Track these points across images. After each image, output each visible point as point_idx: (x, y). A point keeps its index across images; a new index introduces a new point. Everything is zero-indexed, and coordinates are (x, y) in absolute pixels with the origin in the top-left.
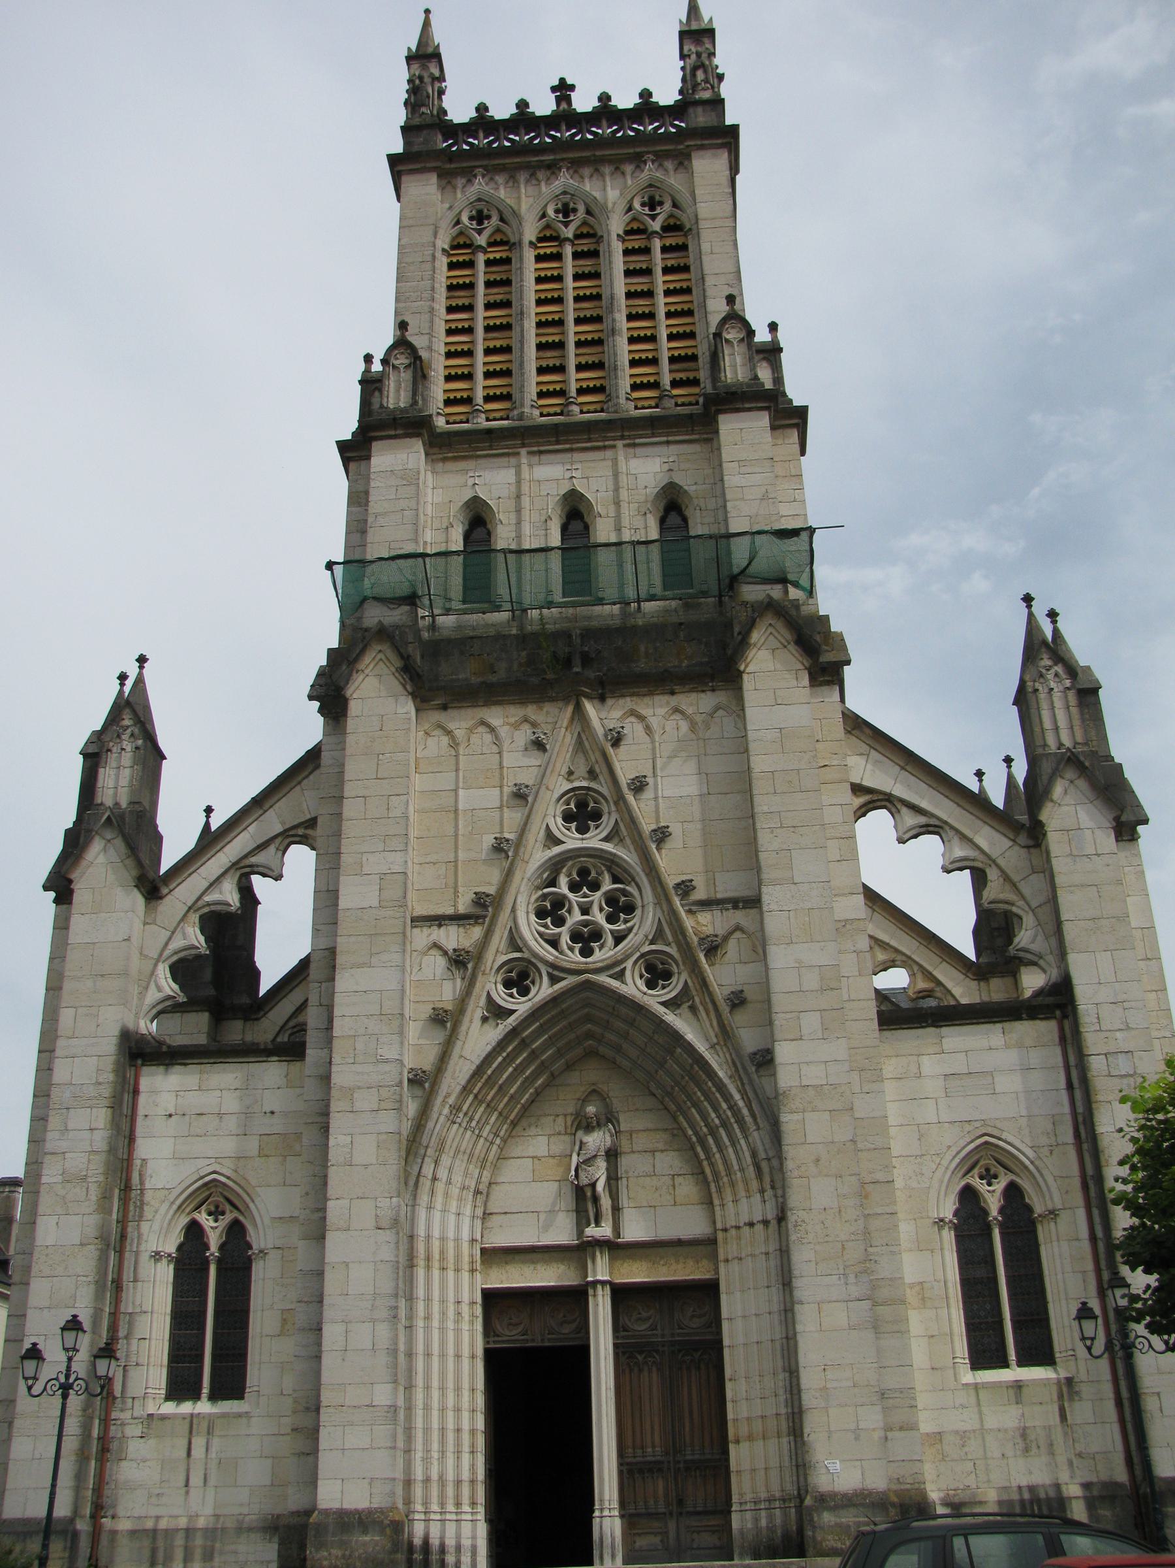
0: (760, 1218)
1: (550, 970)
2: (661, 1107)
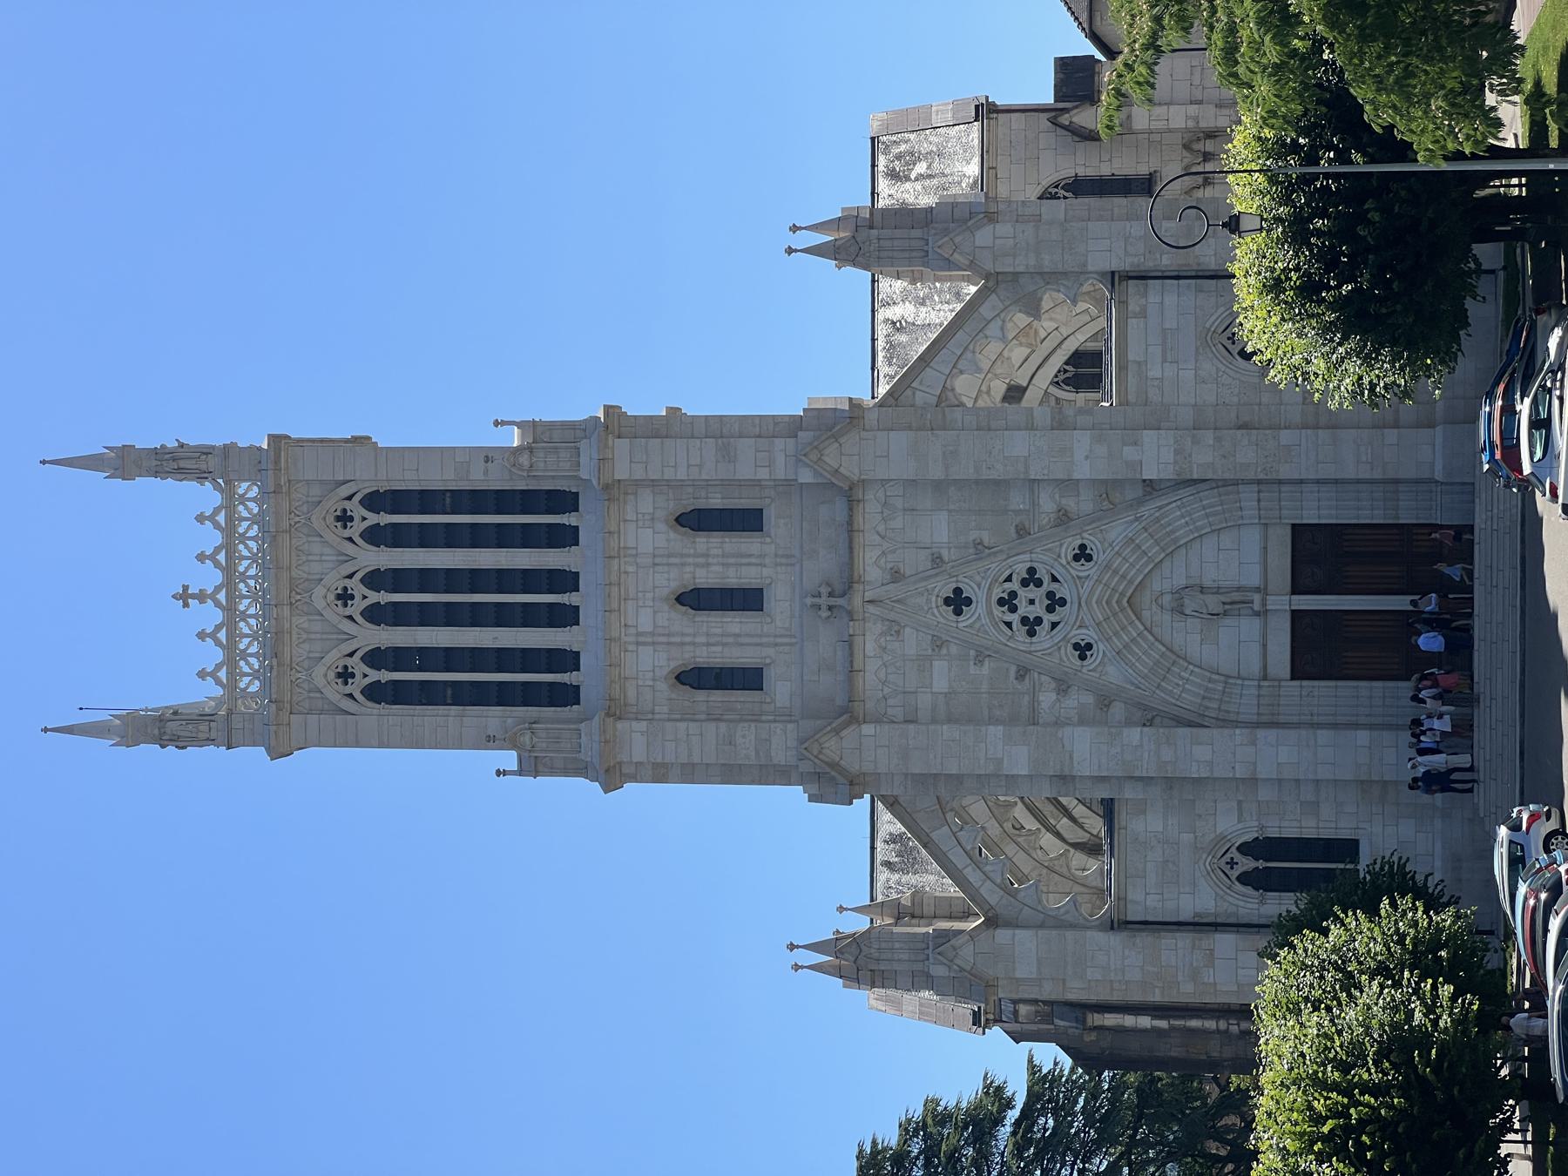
1: (1075, 628)
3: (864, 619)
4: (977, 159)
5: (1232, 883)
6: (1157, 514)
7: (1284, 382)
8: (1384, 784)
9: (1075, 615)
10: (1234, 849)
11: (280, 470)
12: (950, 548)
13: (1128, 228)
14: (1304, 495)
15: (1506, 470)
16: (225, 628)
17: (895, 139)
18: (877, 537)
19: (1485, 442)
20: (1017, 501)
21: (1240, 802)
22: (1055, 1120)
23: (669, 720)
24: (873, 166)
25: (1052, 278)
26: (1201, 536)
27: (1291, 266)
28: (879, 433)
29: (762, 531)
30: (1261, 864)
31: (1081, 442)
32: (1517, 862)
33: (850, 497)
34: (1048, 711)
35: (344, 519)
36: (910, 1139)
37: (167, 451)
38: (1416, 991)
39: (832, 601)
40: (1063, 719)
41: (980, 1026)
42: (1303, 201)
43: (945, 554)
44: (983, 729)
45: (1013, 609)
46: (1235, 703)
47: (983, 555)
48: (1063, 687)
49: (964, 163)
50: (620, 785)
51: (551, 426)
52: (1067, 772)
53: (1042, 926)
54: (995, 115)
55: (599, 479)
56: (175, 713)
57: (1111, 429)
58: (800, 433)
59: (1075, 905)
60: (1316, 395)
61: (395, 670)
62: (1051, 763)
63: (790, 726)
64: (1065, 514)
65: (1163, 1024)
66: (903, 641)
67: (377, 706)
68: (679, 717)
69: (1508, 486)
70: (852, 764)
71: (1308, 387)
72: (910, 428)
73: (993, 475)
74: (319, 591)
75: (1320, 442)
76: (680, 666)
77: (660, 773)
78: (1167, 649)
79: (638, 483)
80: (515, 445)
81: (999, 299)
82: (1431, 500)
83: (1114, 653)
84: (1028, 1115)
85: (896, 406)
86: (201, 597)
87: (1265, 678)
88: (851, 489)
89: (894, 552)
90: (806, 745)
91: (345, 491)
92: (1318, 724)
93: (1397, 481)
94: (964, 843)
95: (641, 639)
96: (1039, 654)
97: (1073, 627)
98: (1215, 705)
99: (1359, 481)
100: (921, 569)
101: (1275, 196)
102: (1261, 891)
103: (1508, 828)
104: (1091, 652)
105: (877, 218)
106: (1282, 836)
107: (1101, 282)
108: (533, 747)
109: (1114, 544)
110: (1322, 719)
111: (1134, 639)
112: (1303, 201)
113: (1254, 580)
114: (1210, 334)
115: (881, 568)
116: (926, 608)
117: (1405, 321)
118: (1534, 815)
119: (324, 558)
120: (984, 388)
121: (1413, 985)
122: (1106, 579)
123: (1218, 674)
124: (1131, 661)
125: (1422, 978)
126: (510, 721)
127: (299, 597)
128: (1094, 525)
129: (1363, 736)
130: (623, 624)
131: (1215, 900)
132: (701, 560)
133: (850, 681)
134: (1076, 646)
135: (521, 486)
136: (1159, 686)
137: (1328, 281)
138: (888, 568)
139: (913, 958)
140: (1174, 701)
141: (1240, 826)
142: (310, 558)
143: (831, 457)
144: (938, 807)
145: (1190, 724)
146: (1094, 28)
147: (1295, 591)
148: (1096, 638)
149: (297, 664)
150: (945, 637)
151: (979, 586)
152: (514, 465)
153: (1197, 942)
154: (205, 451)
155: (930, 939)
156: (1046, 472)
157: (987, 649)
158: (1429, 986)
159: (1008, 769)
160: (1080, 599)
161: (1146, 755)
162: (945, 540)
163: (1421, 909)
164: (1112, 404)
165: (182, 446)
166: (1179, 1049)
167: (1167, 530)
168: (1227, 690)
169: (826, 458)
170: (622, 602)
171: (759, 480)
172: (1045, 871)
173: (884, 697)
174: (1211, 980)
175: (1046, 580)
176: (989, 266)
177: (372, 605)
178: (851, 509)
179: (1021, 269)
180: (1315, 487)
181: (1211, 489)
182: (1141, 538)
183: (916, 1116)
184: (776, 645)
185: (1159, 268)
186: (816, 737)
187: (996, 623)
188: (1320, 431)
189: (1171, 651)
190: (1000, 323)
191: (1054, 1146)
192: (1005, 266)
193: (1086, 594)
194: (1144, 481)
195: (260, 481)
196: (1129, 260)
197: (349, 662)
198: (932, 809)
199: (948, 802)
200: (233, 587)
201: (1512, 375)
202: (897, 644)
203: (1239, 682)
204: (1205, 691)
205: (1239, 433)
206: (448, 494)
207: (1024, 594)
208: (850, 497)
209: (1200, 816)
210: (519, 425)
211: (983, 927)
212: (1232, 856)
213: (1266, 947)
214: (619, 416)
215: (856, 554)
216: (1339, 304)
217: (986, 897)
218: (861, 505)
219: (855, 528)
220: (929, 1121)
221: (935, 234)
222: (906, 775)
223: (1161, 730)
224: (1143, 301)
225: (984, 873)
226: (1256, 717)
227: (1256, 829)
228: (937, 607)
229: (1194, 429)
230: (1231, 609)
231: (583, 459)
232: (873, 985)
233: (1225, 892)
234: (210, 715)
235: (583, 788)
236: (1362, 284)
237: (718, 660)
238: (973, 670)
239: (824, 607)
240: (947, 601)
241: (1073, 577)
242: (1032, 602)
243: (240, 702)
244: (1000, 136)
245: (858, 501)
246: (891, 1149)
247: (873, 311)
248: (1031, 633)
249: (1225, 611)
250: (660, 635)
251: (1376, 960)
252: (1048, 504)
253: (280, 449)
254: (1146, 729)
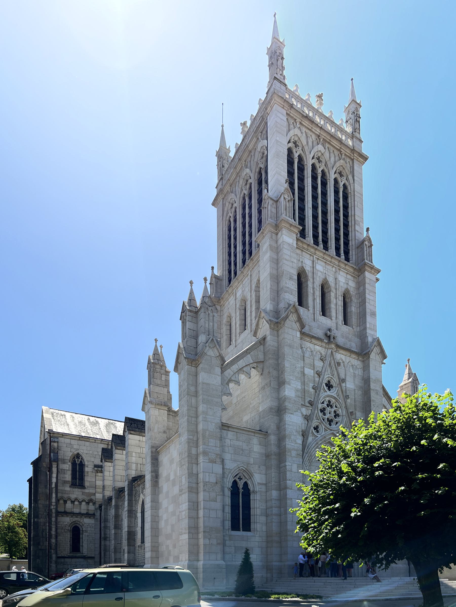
10: (246, 480)
30: (241, 491)
45: (328, 405)
65: (53, 485)
131: (229, 469)
141: (257, 483)
148: (322, 434)
161: (293, 445)
209: (259, 467)
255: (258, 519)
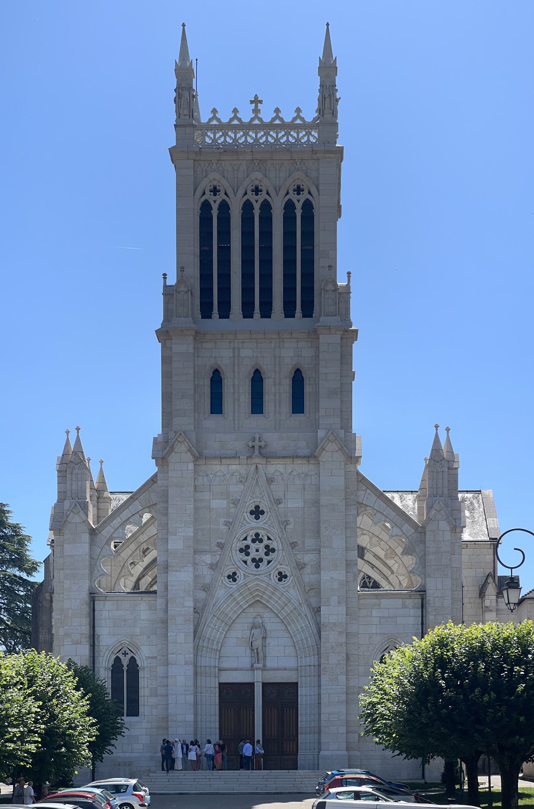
0: (313, 664)
1: (244, 573)
2: (277, 616)
3: (247, 464)
4: (471, 539)
5: (115, 654)
6: (303, 614)
7: (374, 671)
8: (167, 728)
9: (250, 573)
10: (132, 654)
11: (324, 154)
12: (284, 508)
13: (447, 598)
14: (313, 688)
15: (328, 782)
16: (239, 123)
17: (480, 501)
18: (290, 471)
19: (343, 771)
20: (310, 543)
21: (156, 657)
22: (23, 595)
23: (194, 365)
24: (467, 491)
25: (423, 561)
26: (292, 637)
27: (455, 651)
28: (343, 471)
29: (293, 413)
30: (125, 668)
31: (340, 575)
32: (117, 789)
33: (311, 457)
34: (201, 559)
35: (299, 190)
36: (11, 529)
37: (334, 92)
38: (30, 731)
39: (257, 448)
40: (197, 567)
41: (51, 543)
42: (495, 657)
43: (282, 506)
44: (192, 525)
45: (253, 541)
46: (206, 655)
47: (281, 525)
48: (213, 567)
49: (469, 533)
50: (160, 340)
51: (348, 302)
52: (169, 569)
53: (91, 558)
54: (492, 547)
55: (319, 326)
56: (194, 97)
57: (346, 591)
58: (343, 431)
59: (102, 575)
60: (367, 687)
61: (218, 218)
62: (174, 561)
63: (192, 427)
64: (303, 568)
66: (237, 484)
67: (199, 208)
68: (196, 370)
69: (319, 784)
70: (173, 458)
71: (371, 683)
72: (346, 488)
73: (323, 530)
74: (259, 175)
75: (339, 695)
76: (223, 370)
77: (166, 360)
78: (234, 621)
79: (317, 348)
80: (338, 284)
81: (412, 534)
82: (310, 750)
83: (231, 593)
84: (25, 583)
85: (357, 481)
86: (256, 111)
87: (220, 670)
88: (315, 457)
89: (283, 479)
90: (182, 434)
91: (314, 190)
92: (196, 696)
93: (319, 733)
94: (133, 517)
95: (236, 351)
96: (230, 554)
97: (244, 571)
98: (205, 644)
99: (320, 714)
100: (273, 493)
101: (497, 642)
102: (111, 668)
103: (135, 785)
104: (232, 581)
105: (453, 472)
106: (140, 679)
107: (420, 586)
108: (179, 292)
109: (287, 593)
110: (199, 698)
111: (239, 604)
112: (495, 657)
113: (270, 664)
114: (394, 640)
115: (274, 472)
116: (254, 496)
117: (423, 717)
118: (142, 798)
119: (278, 179)
120: (365, 532)
121: (35, 730)
122: (269, 588)
123: (221, 646)
124: (227, 602)
125: (40, 735)
126: (193, 280)
127: (256, 164)
128: (297, 582)
129: (190, 718)
130: (244, 341)
131: (106, 645)
132: (277, 382)
133: (215, 458)
134: (235, 574)
135: (316, 287)
136: (214, 616)
137: (446, 673)
138: (274, 476)
139: (73, 491)
140: (207, 623)
141: (144, 658)
142: (278, 171)
143: (331, 447)
144: (152, 504)
145: (195, 632)
146: (527, 600)
147: (264, 685)
148: (239, 583)
149: (220, 164)
150: (238, 506)
151: (265, 523)
152: (327, 282)
153: (84, 636)
154: (334, 112)
155: (83, 500)
156: (324, 557)
157: (233, 527)
158: (37, 739)
159: (171, 539)
160: (259, 575)
161: (179, 609)
162: (289, 506)
163: (91, 740)
164: (359, 591)
165: (337, 100)
166: (43, 639)
167: (295, 620)
168: (213, 651)
169: (330, 444)
170: (255, 340)
171: (319, 411)
172: (122, 564)
173: (208, 475)
174: (65, 643)
175: (269, 558)
176: (429, 528)
177: (252, 206)
178: (304, 457)
179: (427, 545)
180: (316, 693)
181: (316, 642)
182: (290, 606)
183: (22, 532)
184: (234, 420)
185: (427, 614)
186: (186, 439)
187: (246, 532)
188: (345, 695)
189: (233, 623)
190: (400, 534)
191: (10, 592)
192: (429, 536)
193: (262, 579)
194: (320, 608)
195: (319, 143)
196: (431, 599)
197: (222, 193)
198: (151, 501)
199: (154, 509)
200: (262, 128)
201: (381, 784)
202: (235, 481)
203: (217, 657)
204: (212, 640)
205: (345, 655)
206: (312, 248)
207: (261, 546)
208: (311, 457)
209: (149, 637)
210: (348, 286)
211: (90, 527)
212: (129, 653)
213: (74, 663)
214: (352, 338)
215: (282, 460)
216: (433, 679)
217: (105, 530)
218: (307, 462)
219: (295, 460)
220: (19, 537)
221: (445, 501)
222: (167, 487)
223: (192, 617)
224: (410, 606)
225: (118, 528)
226: (199, 665)
227: (143, 666)
228: (254, 502)
229: (346, 633)
230: (254, 653)
231: (330, 319)
232: (59, 471)
233: (110, 651)
234: (193, 116)
235: (158, 320)
236: (445, 692)
237: (226, 390)
238: (222, 520)
239: (254, 443)
240: (257, 507)
241: (270, 572)
242: (257, 551)
243: (200, 132)
244: (483, 550)
245: (308, 461)
246: (7, 520)
247: (398, 492)
248: (241, 551)
249: (253, 649)
250: (238, 360)
251: (59, 713)
252: (308, 558)
253: (336, 154)
254: (192, 609)
255: (146, 701)
